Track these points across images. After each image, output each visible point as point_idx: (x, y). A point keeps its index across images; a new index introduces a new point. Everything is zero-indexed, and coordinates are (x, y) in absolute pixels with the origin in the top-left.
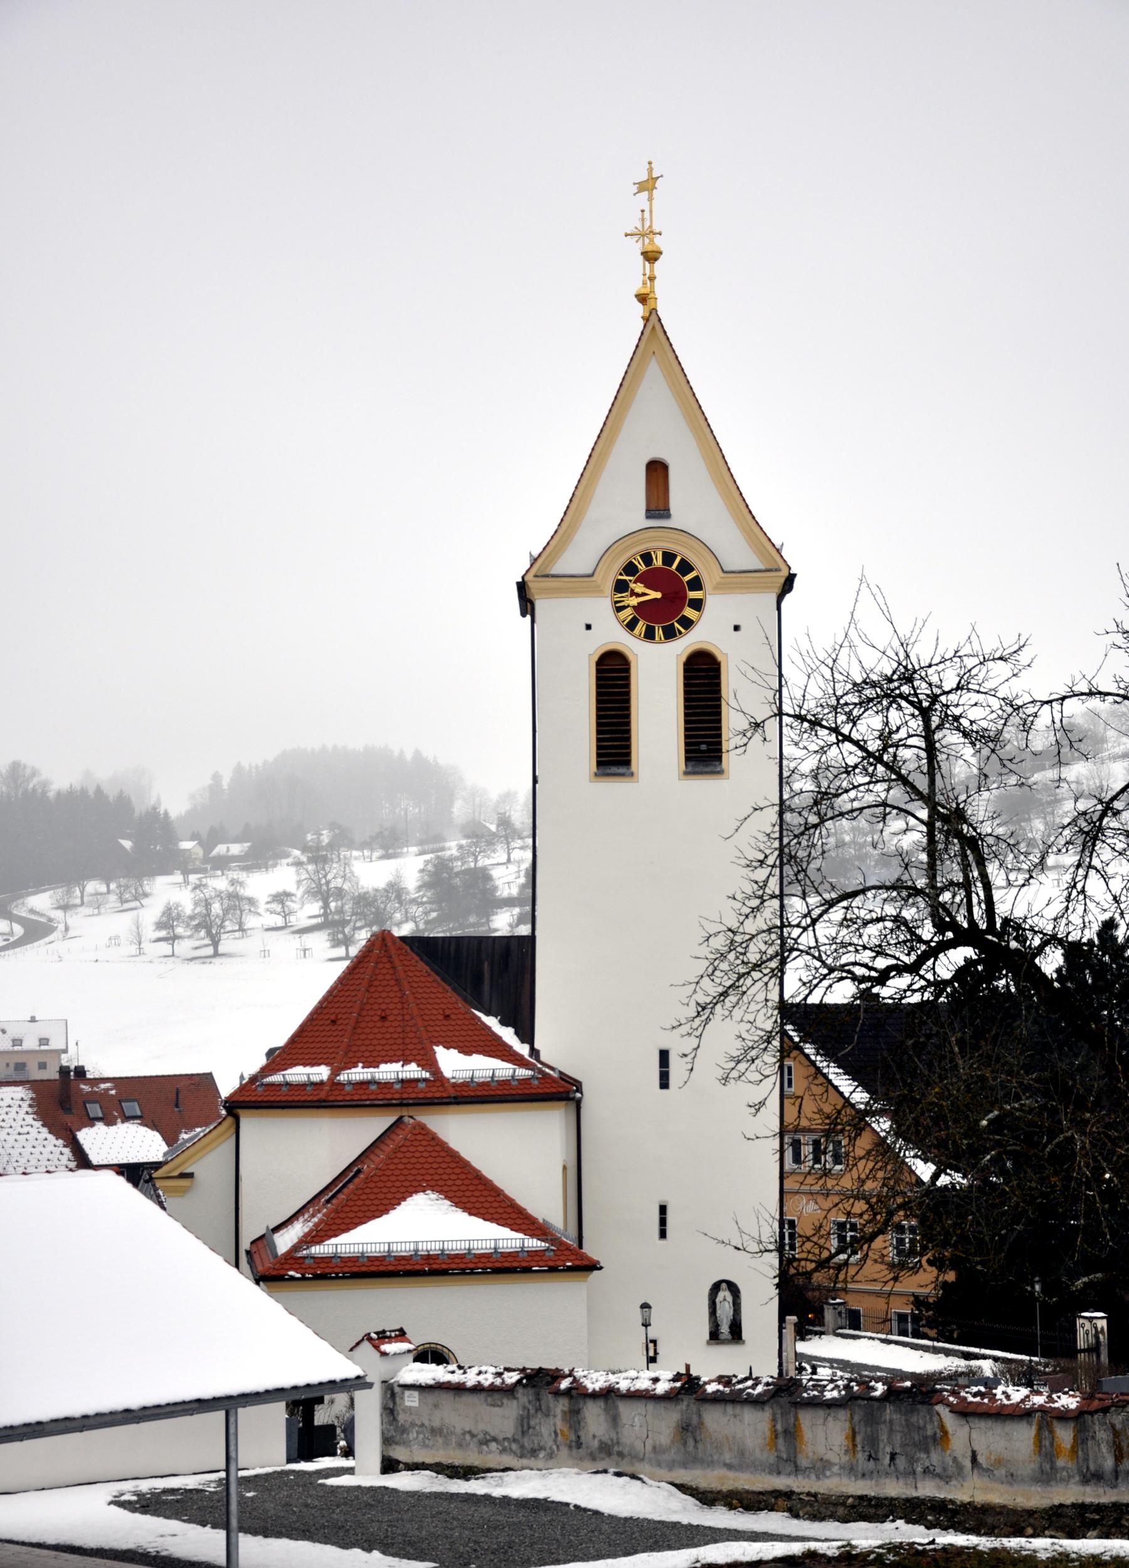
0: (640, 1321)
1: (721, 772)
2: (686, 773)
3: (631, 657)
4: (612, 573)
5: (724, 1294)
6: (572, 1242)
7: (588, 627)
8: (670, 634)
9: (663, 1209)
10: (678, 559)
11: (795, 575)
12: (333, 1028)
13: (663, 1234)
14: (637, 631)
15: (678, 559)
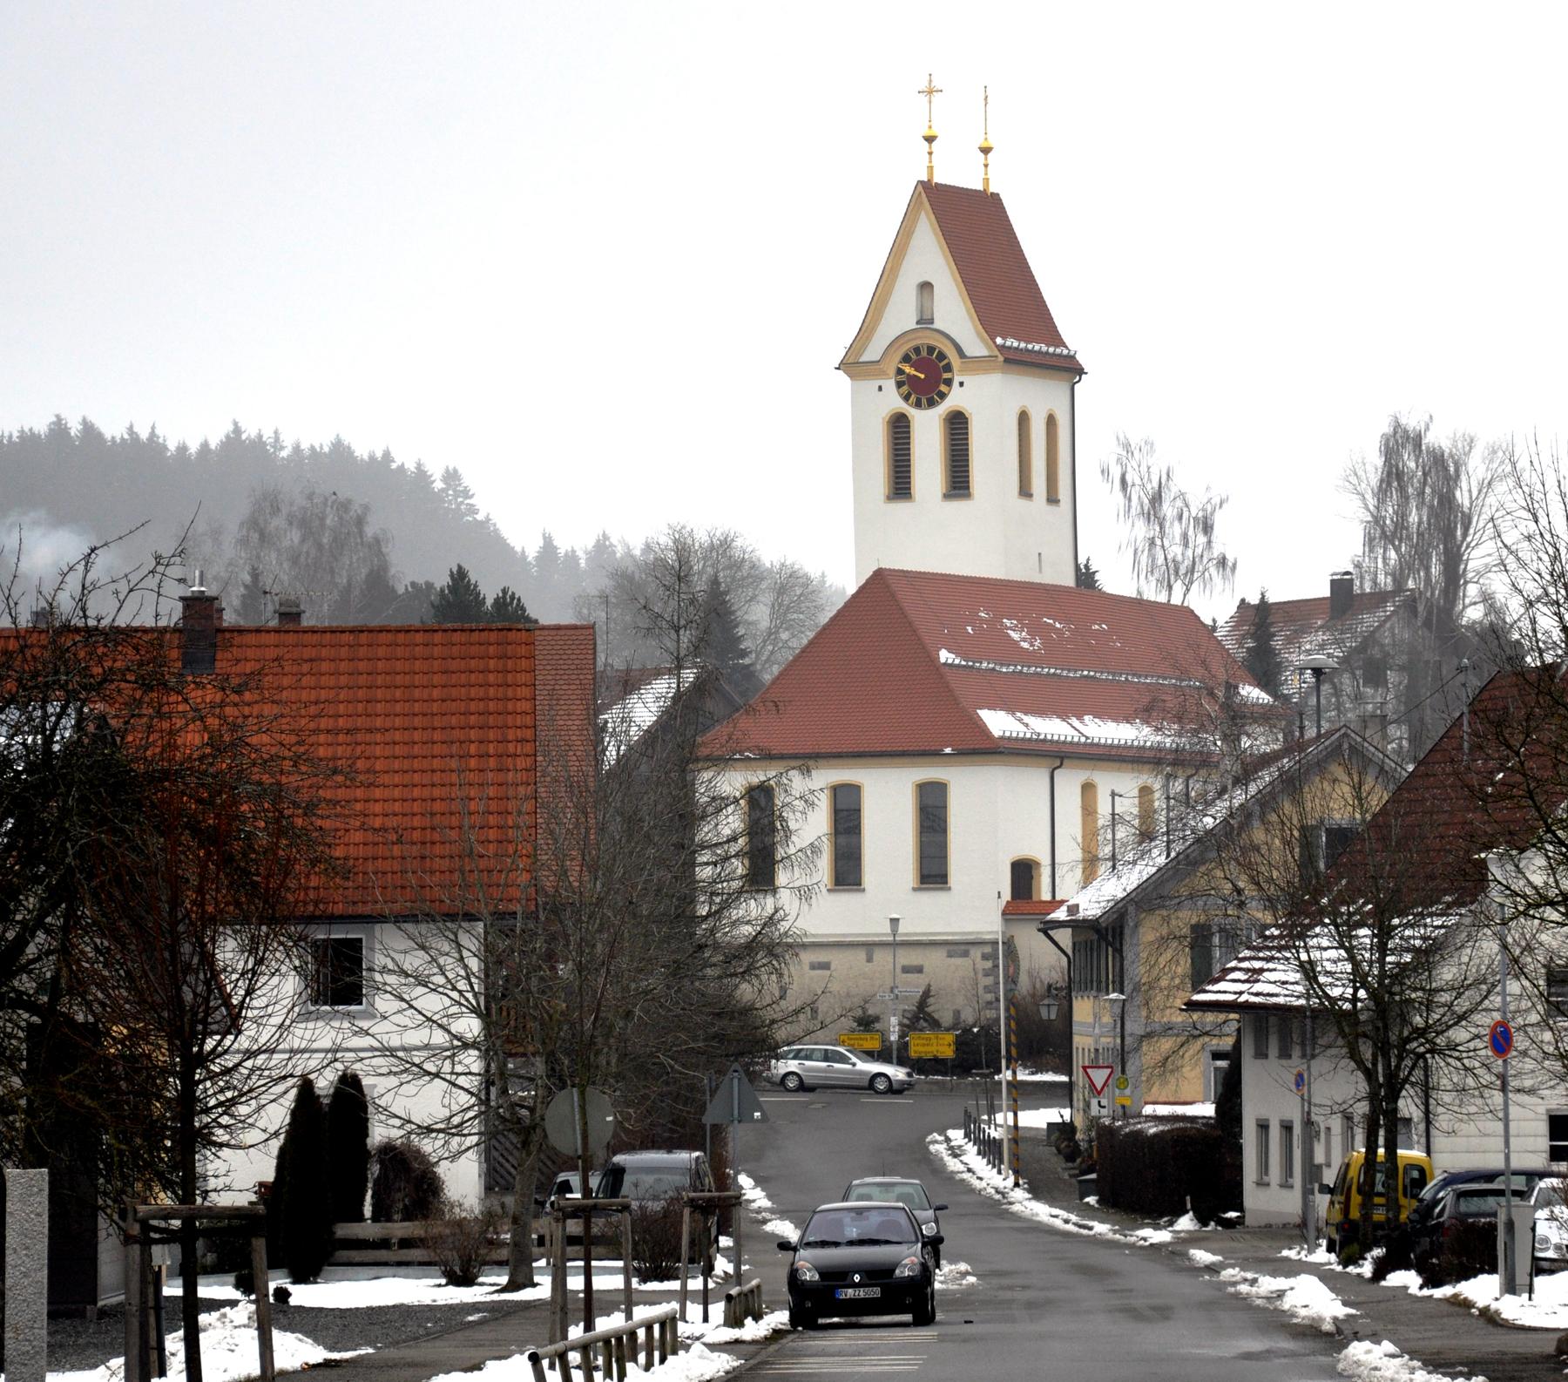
4: (894, 362)
8: (932, 404)
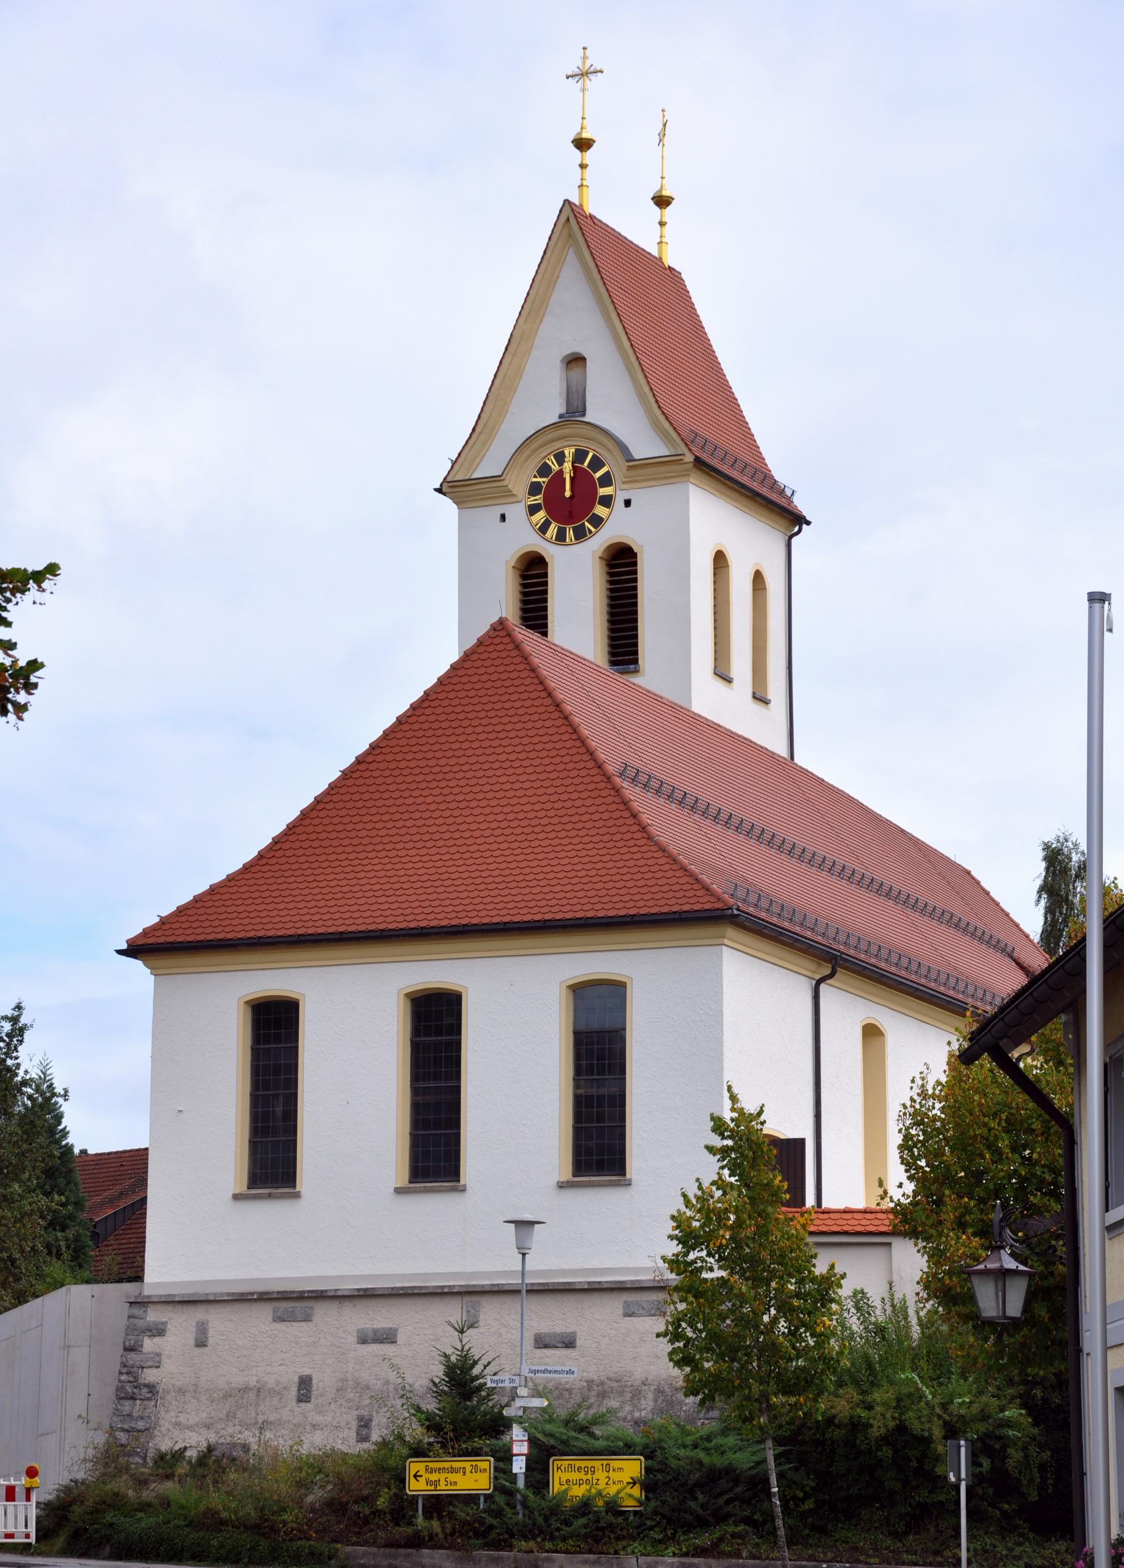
6: (783, 752)
10: (590, 455)
14: (548, 535)
15: (590, 455)
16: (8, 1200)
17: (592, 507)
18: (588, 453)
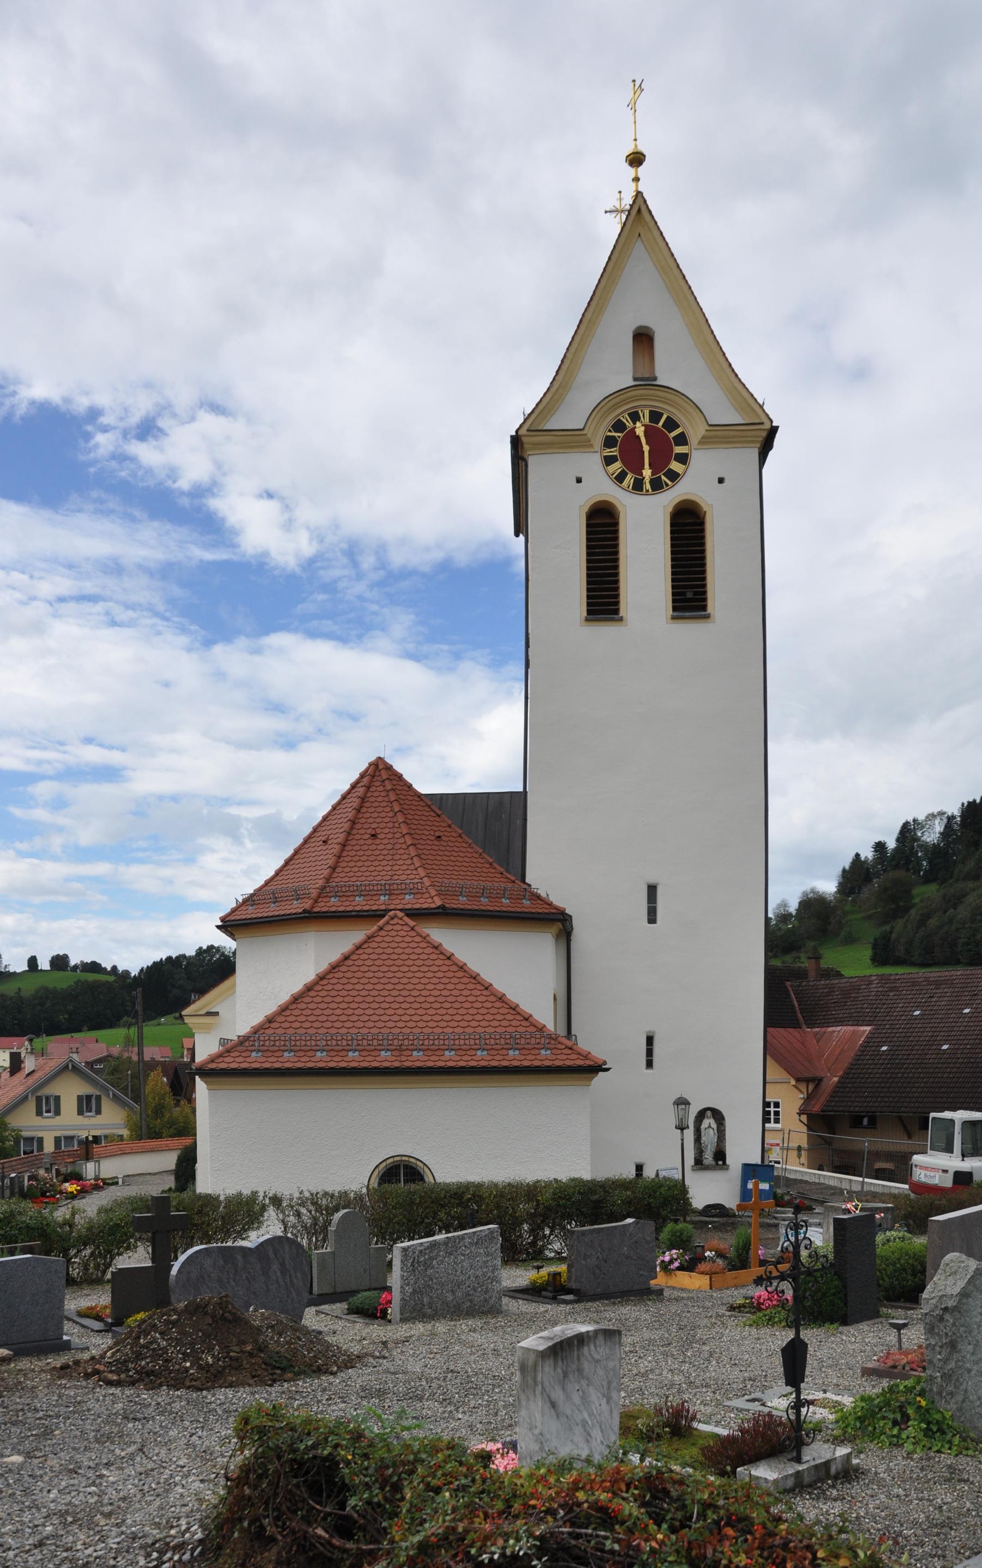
0: (673, 1122)
1: (707, 617)
2: (673, 618)
3: (620, 508)
5: (708, 1122)
7: (579, 480)
9: (650, 1040)
10: (665, 417)
11: (777, 427)
12: (325, 848)
13: (650, 1064)
15: (665, 417)
16: (3, 1379)
17: (669, 462)
18: (662, 414)
